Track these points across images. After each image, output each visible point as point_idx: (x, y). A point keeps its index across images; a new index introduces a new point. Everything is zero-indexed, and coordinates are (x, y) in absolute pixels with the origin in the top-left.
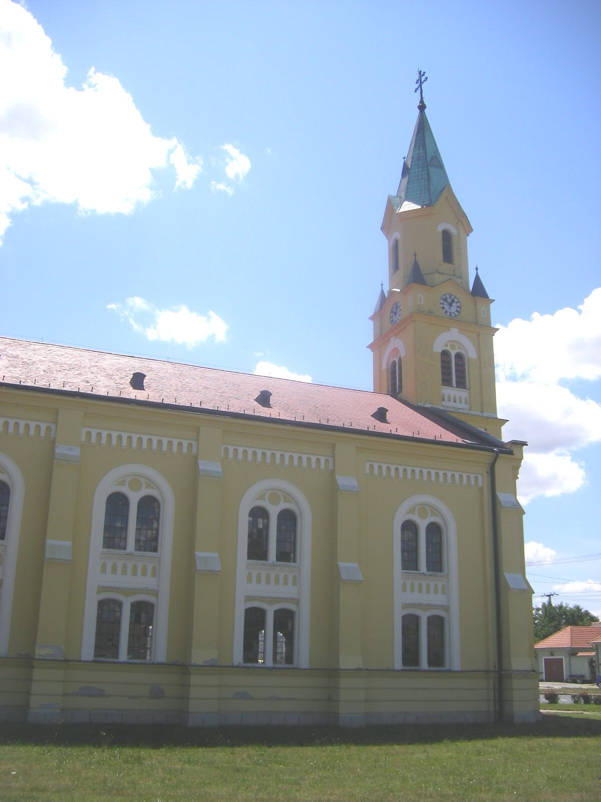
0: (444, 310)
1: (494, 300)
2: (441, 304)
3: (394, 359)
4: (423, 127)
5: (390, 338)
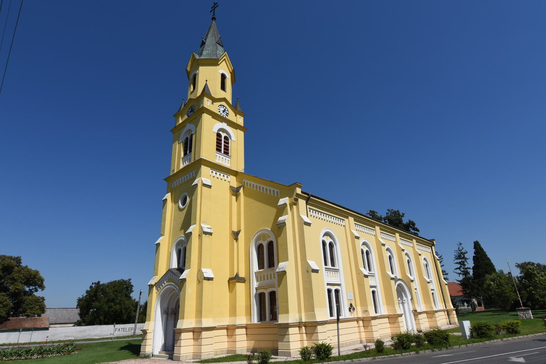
2: (219, 109)
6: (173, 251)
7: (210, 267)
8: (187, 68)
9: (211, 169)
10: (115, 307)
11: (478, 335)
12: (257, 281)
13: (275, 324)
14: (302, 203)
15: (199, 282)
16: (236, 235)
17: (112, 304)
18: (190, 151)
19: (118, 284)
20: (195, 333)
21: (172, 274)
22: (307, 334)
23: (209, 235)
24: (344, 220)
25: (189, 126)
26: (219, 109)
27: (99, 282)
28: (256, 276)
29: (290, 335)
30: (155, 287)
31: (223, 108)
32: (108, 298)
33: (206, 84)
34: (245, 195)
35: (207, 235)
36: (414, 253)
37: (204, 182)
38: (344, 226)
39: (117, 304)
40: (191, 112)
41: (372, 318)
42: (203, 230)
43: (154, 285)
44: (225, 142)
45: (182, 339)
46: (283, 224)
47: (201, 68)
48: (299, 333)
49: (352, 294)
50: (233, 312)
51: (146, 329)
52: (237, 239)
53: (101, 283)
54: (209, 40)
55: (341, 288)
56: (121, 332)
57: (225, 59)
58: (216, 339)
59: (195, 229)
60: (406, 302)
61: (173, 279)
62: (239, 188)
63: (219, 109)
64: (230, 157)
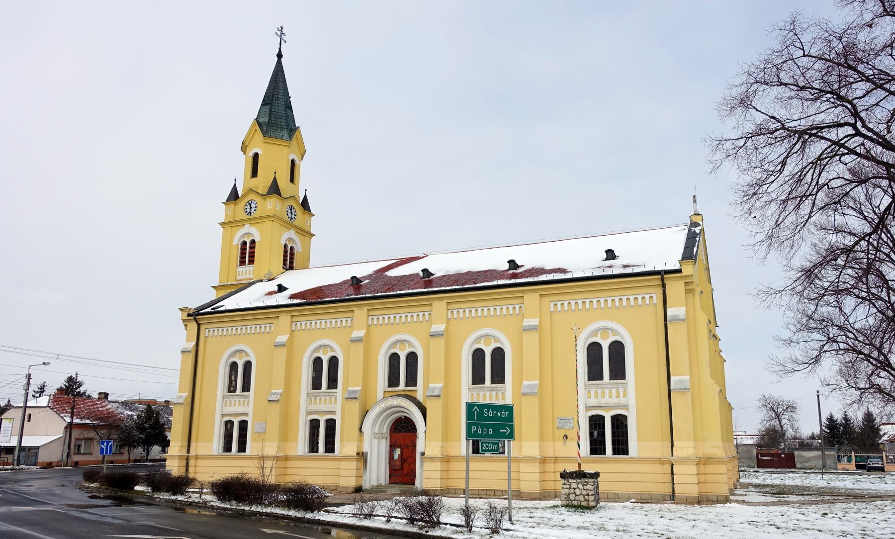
1: (288, 289)
4: (278, 76)
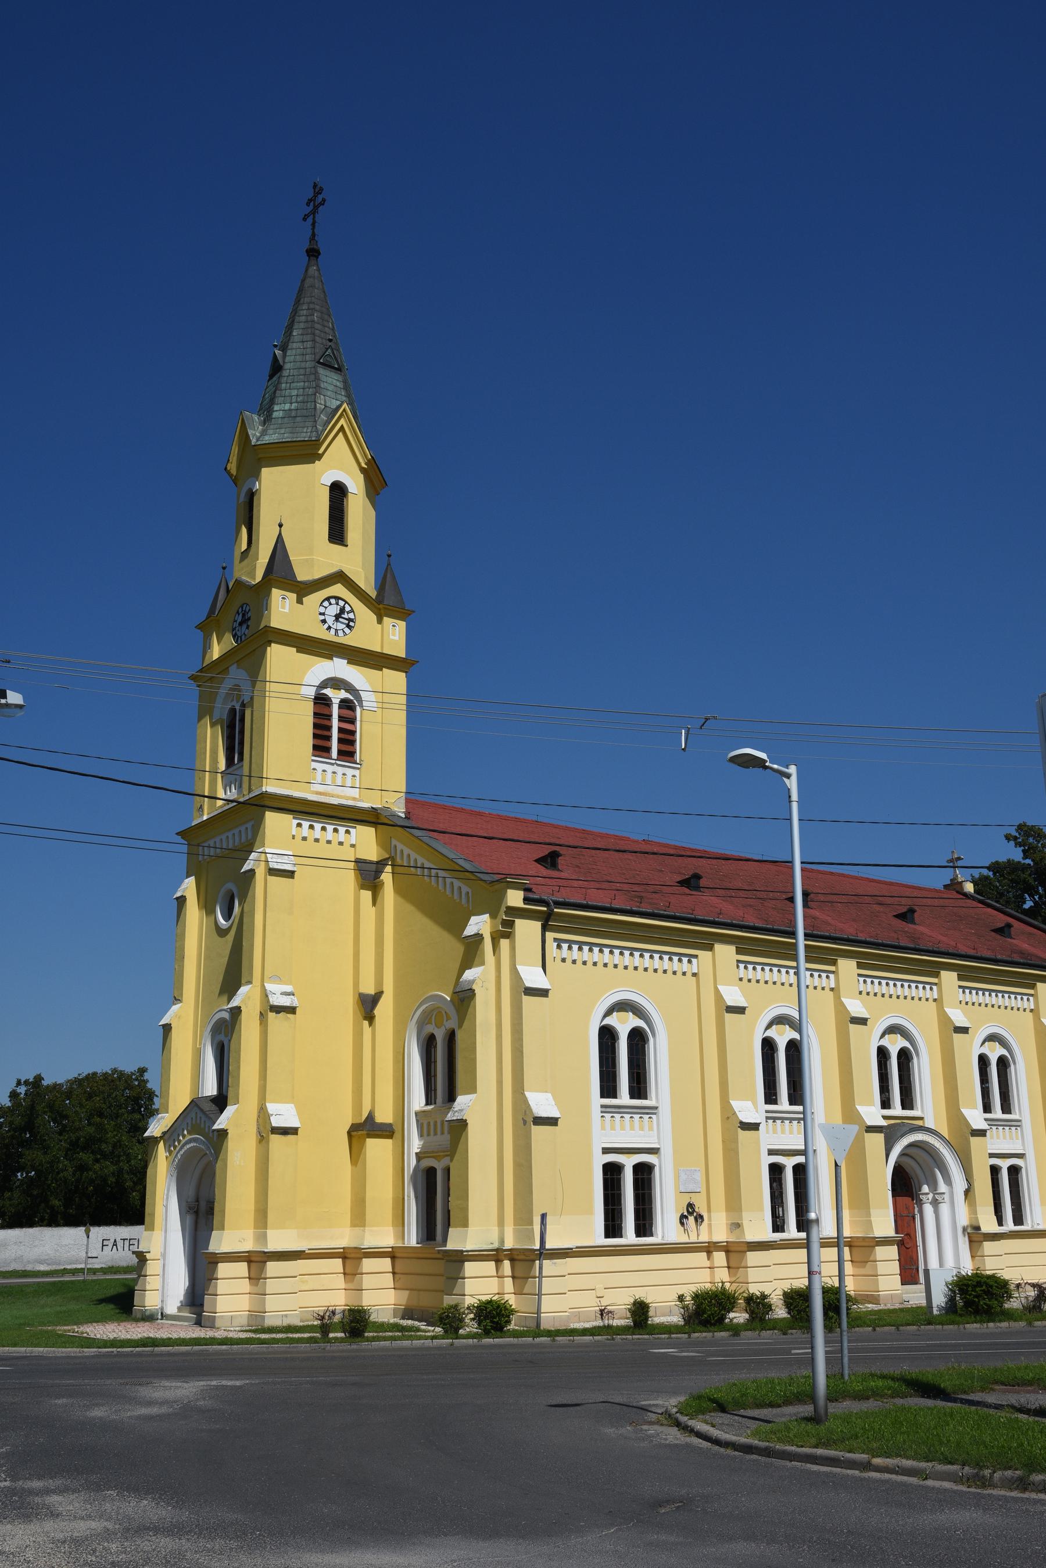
0: (326, 626)
2: (321, 614)
3: (234, 703)
5: (228, 668)
6: (204, 1046)
7: (291, 1099)
8: (229, 465)
9: (294, 818)
10: (97, 1166)
11: (968, 1304)
12: (421, 1135)
13: (439, 1250)
14: (528, 930)
15: (262, 1139)
16: (368, 1005)
17: (85, 1157)
18: (241, 759)
19: (104, 1085)
20: (253, 1265)
21: (200, 1114)
22: (515, 1280)
23: (288, 1013)
24: (696, 956)
25: (236, 674)
26: (323, 614)
27: (39, 1079)
28: (417, 1121)
29: (466, 1280)
30: (162, 1143)
31: (337, 604)
32: (73, 1137)
33: (280, 539)
34: (398, 890)
35: (282, 1014)
36: (1035, 1029)
37: (273, 865)
38: (694, 975)
39: (105, 1156)
40: (241, 624)
41: (748, 1247)
42: (268, 1001)
43: (160, 1137)
44: (341, 719)
45: (219, 1277)
46: (469, 993)
47: (265, 471)
48: (496, 1275)
49: (700, 1176)
50: (359, 1217)
51: (144, 1251)
52: (370, 1018)
53: (45, 1083)
54: (294, 352)
55: (659, 1158)
56: (123, 1253)
57: (342, 428)
58: (312, 1282)
59: (249, 998)
60: (946, 1197)
61: (202, 1126)
62: (380, 865)
63: (323, 614)
64: (359, 766)
